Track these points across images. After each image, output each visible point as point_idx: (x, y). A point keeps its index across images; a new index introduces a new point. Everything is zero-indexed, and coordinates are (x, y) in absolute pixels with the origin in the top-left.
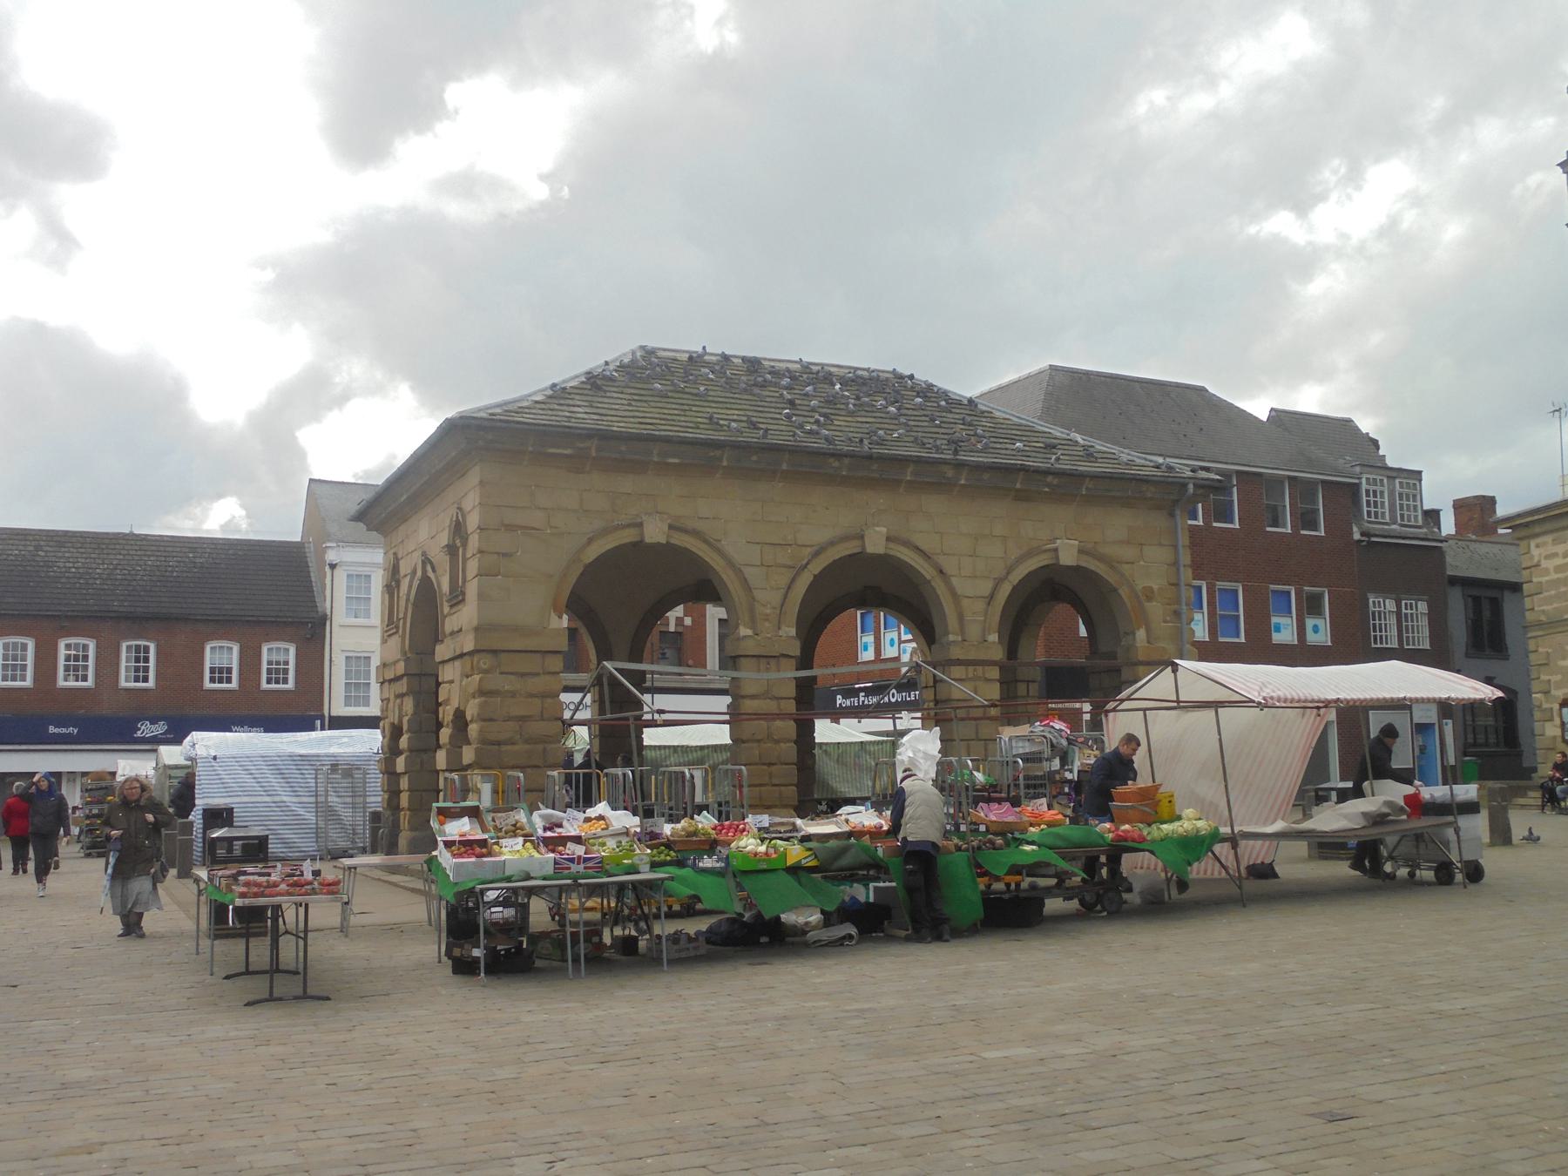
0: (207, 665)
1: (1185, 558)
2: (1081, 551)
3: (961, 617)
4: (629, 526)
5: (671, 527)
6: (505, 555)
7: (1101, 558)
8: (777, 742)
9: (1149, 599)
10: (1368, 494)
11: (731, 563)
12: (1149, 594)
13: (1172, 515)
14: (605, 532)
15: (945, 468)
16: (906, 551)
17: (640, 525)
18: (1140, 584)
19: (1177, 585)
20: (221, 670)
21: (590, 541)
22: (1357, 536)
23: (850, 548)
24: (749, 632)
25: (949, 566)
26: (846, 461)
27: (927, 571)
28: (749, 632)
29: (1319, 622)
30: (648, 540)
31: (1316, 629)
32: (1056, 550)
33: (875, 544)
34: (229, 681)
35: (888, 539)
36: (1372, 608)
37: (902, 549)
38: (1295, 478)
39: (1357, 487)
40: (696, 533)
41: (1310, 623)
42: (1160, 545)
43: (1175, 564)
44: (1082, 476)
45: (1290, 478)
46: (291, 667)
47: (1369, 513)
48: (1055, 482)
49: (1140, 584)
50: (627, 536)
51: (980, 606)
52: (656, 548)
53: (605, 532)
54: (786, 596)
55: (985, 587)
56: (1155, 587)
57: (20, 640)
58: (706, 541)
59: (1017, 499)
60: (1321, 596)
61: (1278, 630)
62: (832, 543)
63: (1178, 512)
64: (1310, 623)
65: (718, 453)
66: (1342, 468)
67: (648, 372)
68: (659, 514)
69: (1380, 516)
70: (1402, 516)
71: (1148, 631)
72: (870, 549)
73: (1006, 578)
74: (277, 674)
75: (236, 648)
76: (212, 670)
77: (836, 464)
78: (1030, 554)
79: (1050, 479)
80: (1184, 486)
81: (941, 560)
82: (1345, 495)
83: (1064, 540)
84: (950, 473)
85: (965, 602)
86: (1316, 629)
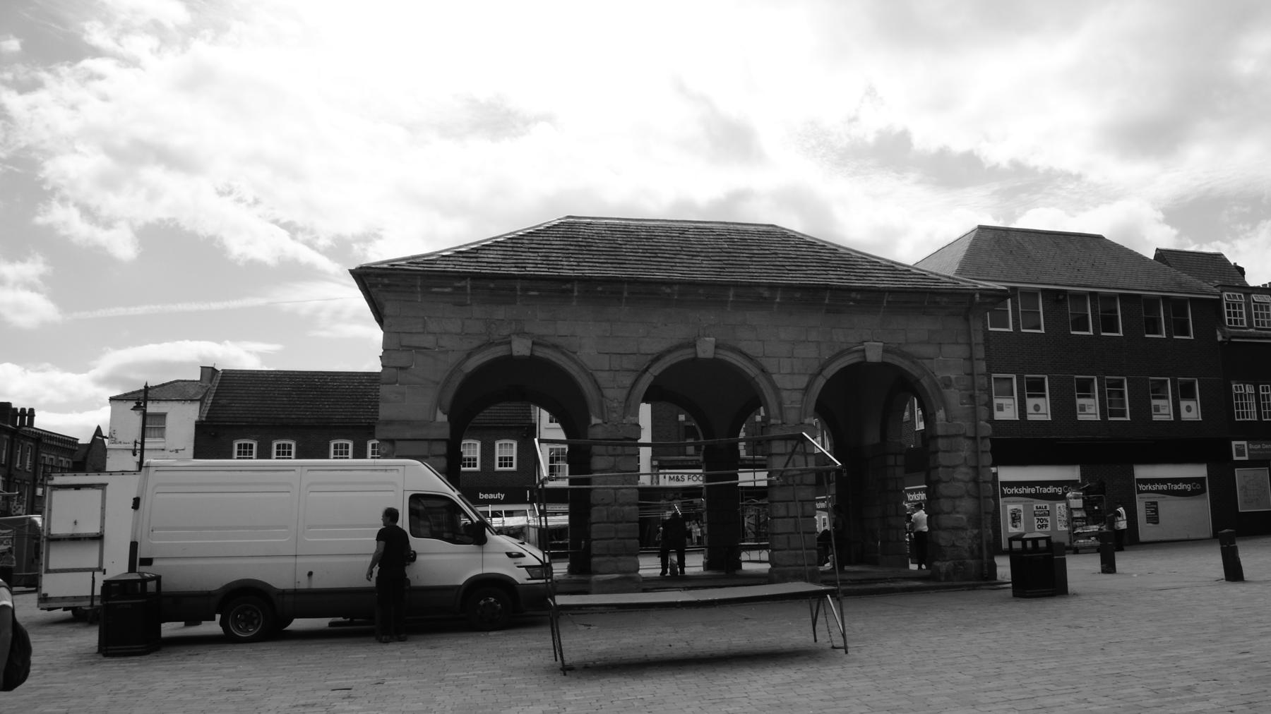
0: (497, 456)
1: (980, 352)
2: (886, 350)
3: (780, 405)
4: (500, 344)
5: (534, 343)
6: (401, 368)
7: (905, 355)
8: (622, 505)
9: (948, 386)
10: (1228, 307)
11: (583, 368)
12: (948, 383)
13: (967, 319)
14: (479, 348)
15: (761, 290)
16: (734, 356)
17: (510, 343)
18: (940, 375)
19: (971, 374)
20: (506, 459)
21: (469, 355)
22: (1220, 338)
23: (685, 354)
24: (599, 421)
25: (770, 365)
26: (676, 288)
27: (751, 371)
28: (599, 421)
29: (1192, 404)
30: (515, 354)
31: (1189, 409)
32: (864, 350)
33: (706, 349)
34: (475, 465)
35: (716, 347)
36: (1234, 391)
37: (730, 354)
38: (1096, 293)
39: (1221, 300)
40: (555, 347)
41: (1184, 404)
42: (957, 343)
43: (970, 358)
44: (850, 290)
45: (1091, 293)
46: (515, 456)
47: (1230, 321)
48: (859, 297)
49: (940, 375)
50: (499, 351)
51: (797, 396)
52: (522, 360)
53: (479, 348)
54: (629, 394)
55: (802, 381)
56: (953, 377)
57: (287, 442)
58: (563, 353)
59: (828, 311)
60: (1193, 384)
61: (1000, 408)
62: (669, 351)
63: (971, 317)
64: (1184, 404)
65: (569, 286)
66: (1208, 288)
67: (571, 236)
68: (524, 333)
69: (1237, 324)
70: (1257, 322)
71: (946, 411)
72: (701, 355)
73: (820, 373)
74: (506, 461)
75: (479, 444)
76: (500, 459)
77: (668, 290)
78: (841, 354)
79: (853, 295)
80: (973, 295)
81: (764, 362)
82: (1210, 309)
83: (873, 344)
84: (766, 294)
85: (785, 394)
86: (1189, 409)
